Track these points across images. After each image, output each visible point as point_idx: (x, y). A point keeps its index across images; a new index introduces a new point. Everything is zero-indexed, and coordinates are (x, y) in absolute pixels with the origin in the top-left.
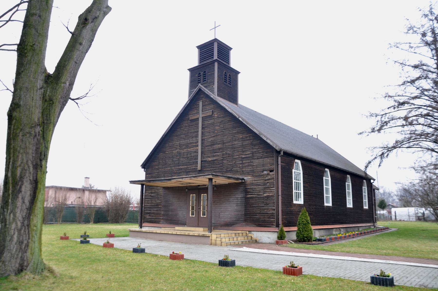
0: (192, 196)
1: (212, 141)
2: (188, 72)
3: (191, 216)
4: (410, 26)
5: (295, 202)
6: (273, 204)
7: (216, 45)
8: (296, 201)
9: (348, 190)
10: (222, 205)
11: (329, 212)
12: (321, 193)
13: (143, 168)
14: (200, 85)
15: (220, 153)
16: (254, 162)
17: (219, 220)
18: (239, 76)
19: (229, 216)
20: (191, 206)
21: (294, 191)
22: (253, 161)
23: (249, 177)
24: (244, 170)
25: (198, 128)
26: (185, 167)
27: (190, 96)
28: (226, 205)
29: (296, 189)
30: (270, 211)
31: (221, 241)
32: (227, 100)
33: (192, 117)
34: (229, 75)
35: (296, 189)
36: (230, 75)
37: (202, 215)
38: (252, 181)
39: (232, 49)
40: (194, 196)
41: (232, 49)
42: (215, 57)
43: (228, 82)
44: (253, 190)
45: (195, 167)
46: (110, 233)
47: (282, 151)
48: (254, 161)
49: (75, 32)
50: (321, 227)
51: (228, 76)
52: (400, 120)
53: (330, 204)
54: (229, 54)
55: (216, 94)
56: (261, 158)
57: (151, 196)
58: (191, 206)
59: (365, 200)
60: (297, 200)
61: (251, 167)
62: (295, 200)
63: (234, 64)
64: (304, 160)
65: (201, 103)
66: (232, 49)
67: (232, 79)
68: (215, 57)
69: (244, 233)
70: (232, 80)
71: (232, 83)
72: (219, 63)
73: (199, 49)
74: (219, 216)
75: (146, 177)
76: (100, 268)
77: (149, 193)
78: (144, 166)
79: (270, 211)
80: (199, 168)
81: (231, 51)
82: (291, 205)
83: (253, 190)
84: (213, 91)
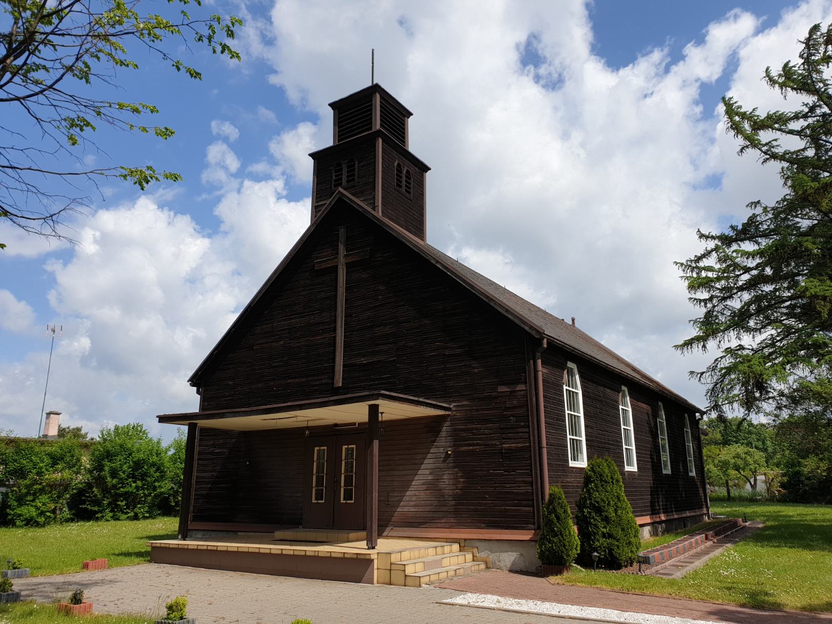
0: (347, 449)
3: (314, 501)
4: (732, 133)
5: (572, 464)
6: (528, 469)
7: (378, 97)
8: (573, 462)
9: (661, 435)
10: (396, 473)
11: (634, 487)
12: (617, 441)
13: (193, 385)
14: (341, 189)
17: (387, 510)
19: (414, 499)
20: (314, 477)
21: (569, 437)
26: (304, 380)
27: (315, 216)
28: (405, 472)
30: (519, 487)
31: (404, 571)
36: (408, 172)
37: (316, 500)
39: (412, 114)
40: (324, 450)
41: (412, 114)
42: (377, 125)
43: (404, 188)
44: (474, 434)
46: (704, 346)
47: (545, 340)
49: (283, 555)
50: (642, 520)
53: (634, 468)
54: (404, 124)
57: (212, 453)
58: (314, 477)
60: (574, 460)
62: (571, 460)
63: (417, 144)
65: (342, 232)
66: (412, 114)
68: (377, 125)
70: (412, 183)
71: (412, 189)
72: (386, 141)
73: (337, 111)
74: (388, 501)
75: (202, 407)
77: (206, 446)
78: (197, 380)
79: (519, 487)
81: (409, 119)
82: (564, 471)
83: (474, 434)
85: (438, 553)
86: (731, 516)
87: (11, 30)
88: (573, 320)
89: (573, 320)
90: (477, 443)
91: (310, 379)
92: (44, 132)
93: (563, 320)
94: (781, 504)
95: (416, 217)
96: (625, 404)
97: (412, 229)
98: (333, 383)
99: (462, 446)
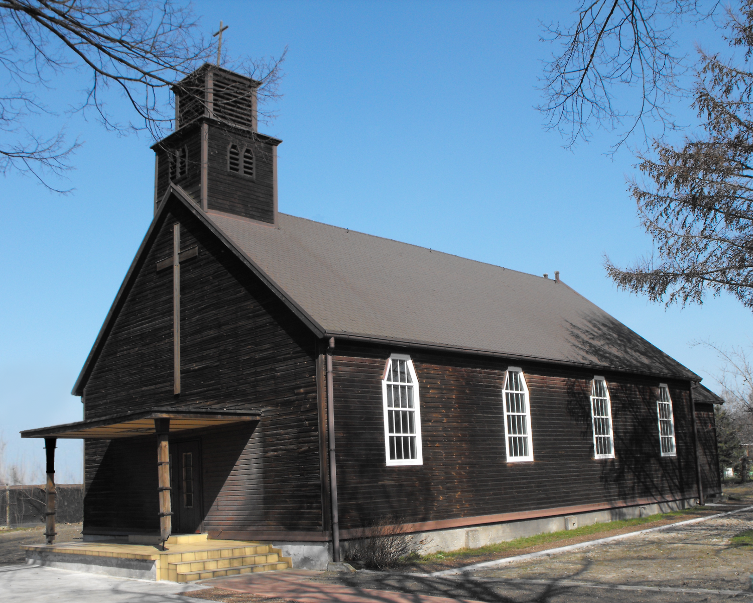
0: (186, 456)
1: (198, 320)
2: (153, 153)
15: (214, 350)
16: (277, 369)
18: (279, 151)
22: (277, 366)
23: (269, 408)
24: (259, 389)
25: (171, 291)
26: (153, 387)
29: (600, 430)
32: (238, 213)
33: (161, 264)
34: (244, 150)
35: (600, 430)
38: (280, 415)
40: (190, 455)
44: (278, 440)
45: (168, 388)
48: (277, 366)
51: (242, 153)
52: (29, 46)
55: (205, 202)
56: (291, 358)
59: (665, 451)
61: (273, 382)
64: (531, 366)
67: (257, 160)
69: (340, 534)
75: (87, 416)
76: (410, 552)
80: (177, 389)
84: (197, 196)
85: (170, 565)
86: (643, 565)
87: (167, 88)
88: (557, 274)
89: (557, 274)
90: (280, 448)
91: (158, 386)
92: (569, 95)
93: (545, 276)
94: (30, 523)
95: (262, 199)
96: (600, 392)
97: (254, 213)
98: (173, 391)
99: (268, 451)
